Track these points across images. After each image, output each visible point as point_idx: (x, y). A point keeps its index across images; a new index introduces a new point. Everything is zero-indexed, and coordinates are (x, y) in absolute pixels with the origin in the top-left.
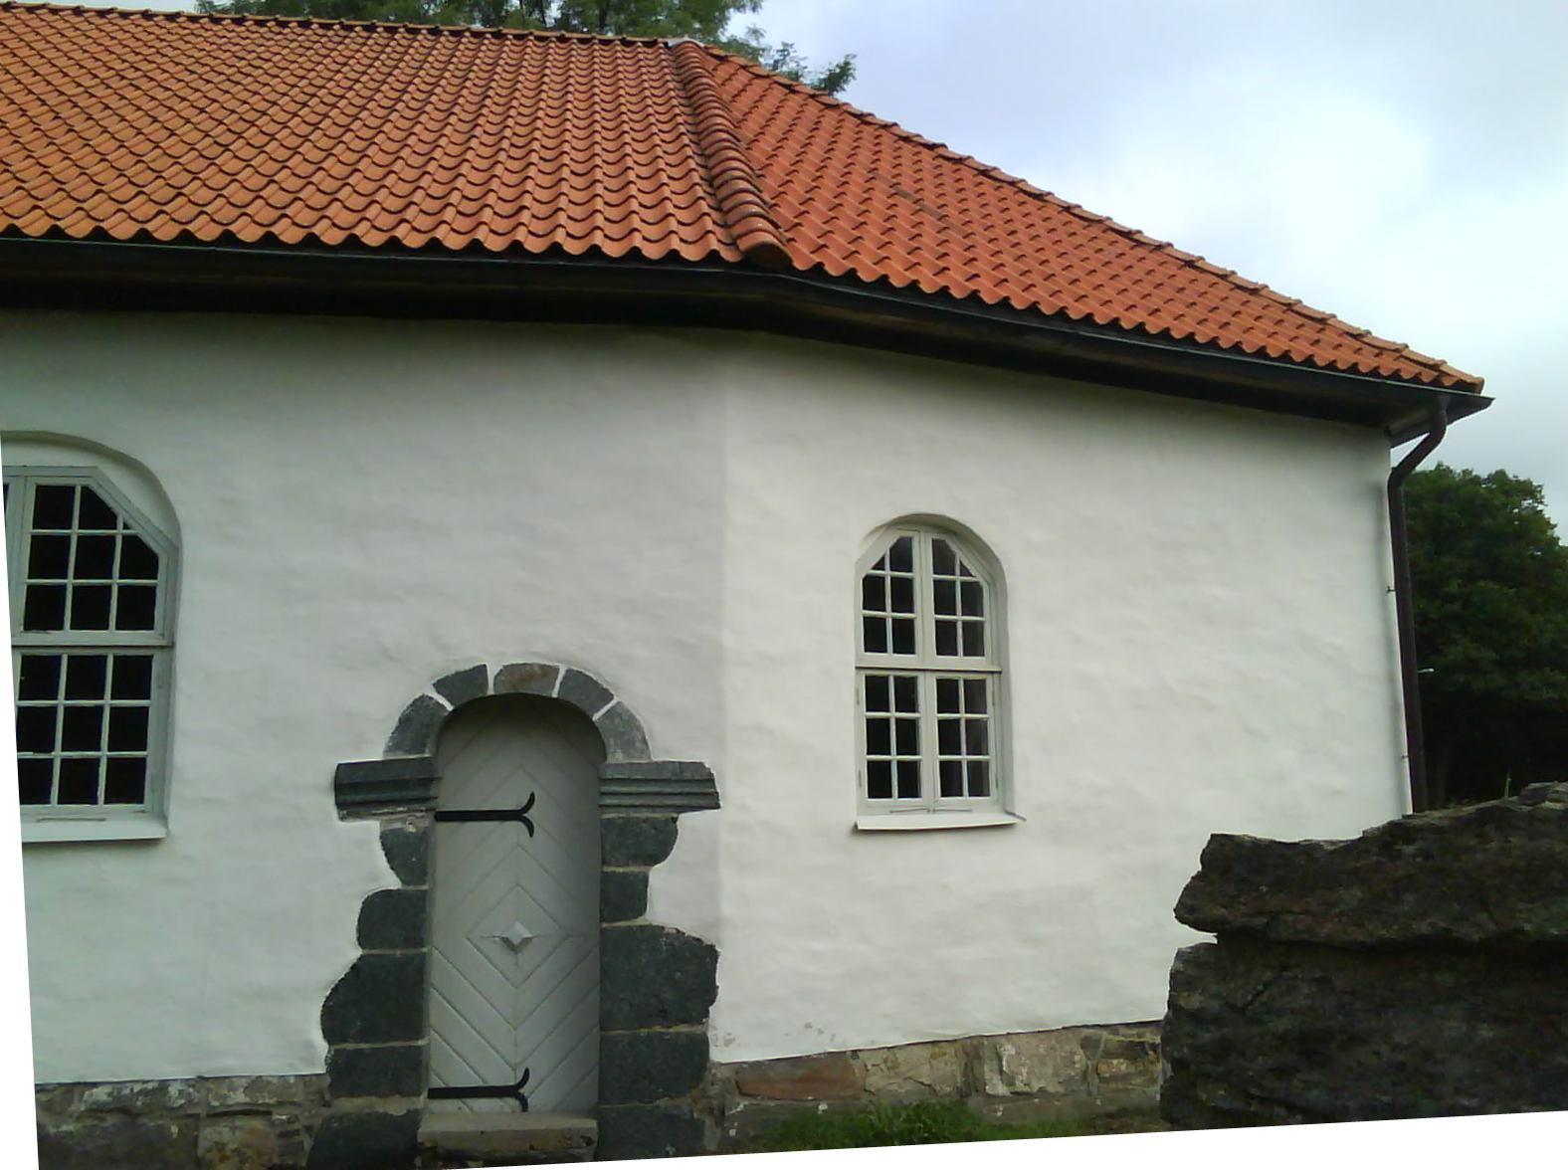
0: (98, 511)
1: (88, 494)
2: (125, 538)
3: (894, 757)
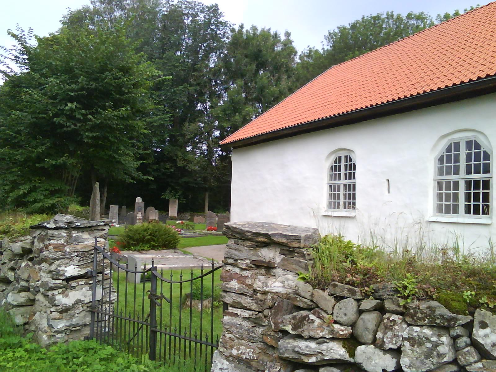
0: (478, 146)
1: (475, 141)
2: (483, 151)
3: (481, 191)
